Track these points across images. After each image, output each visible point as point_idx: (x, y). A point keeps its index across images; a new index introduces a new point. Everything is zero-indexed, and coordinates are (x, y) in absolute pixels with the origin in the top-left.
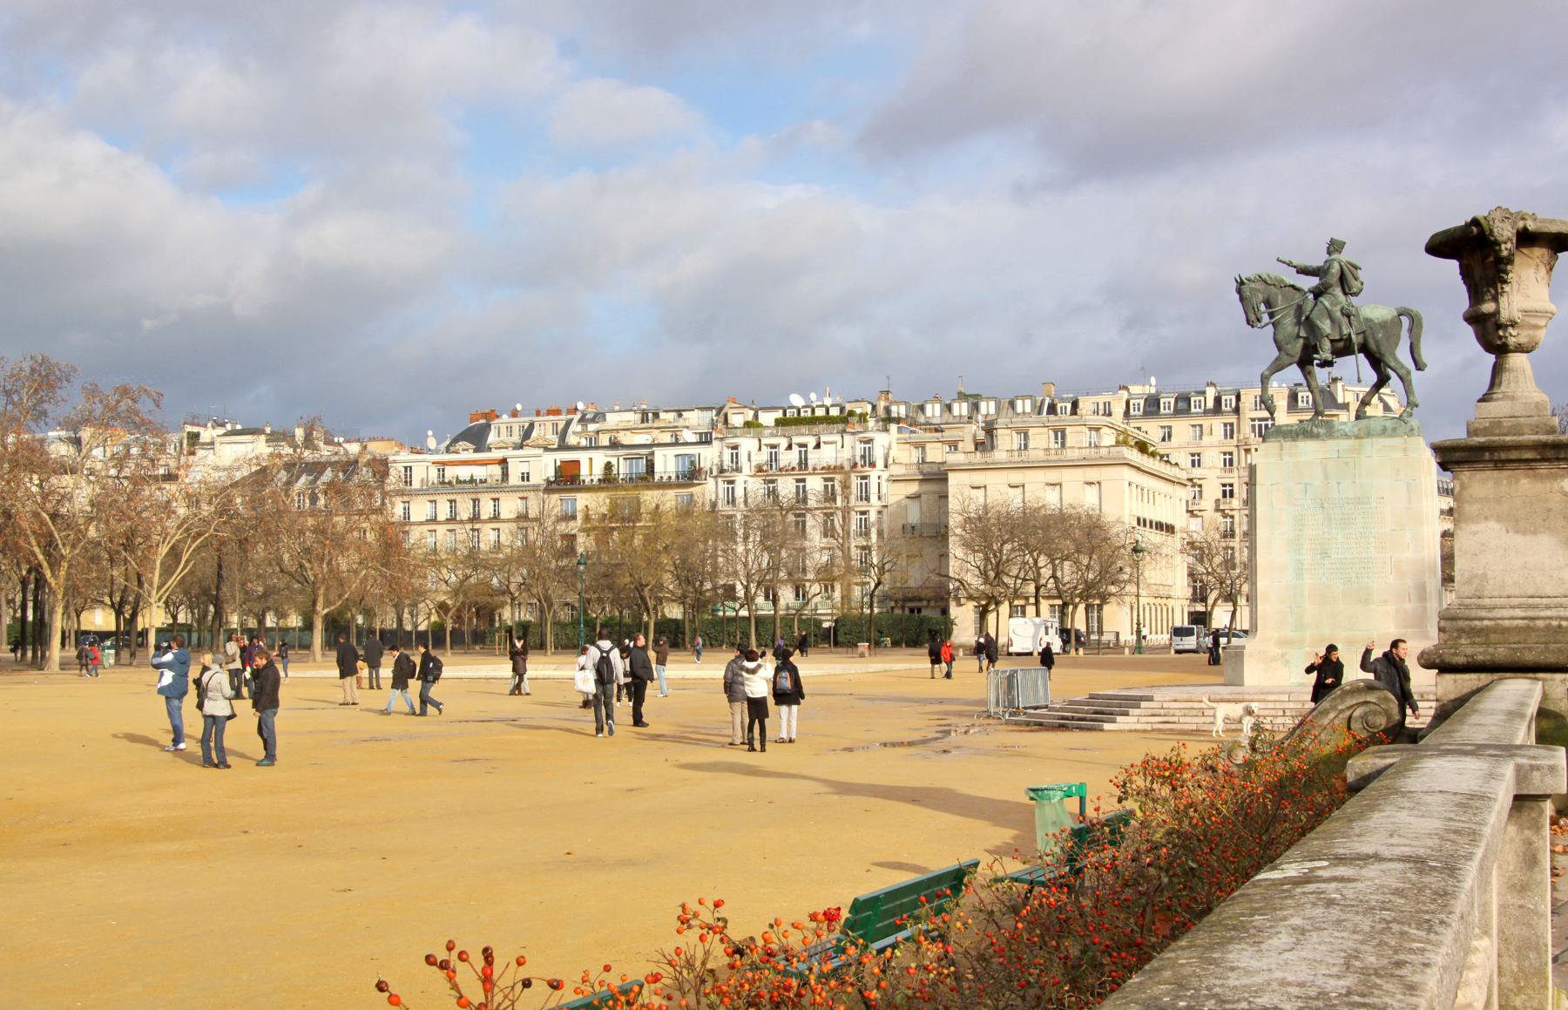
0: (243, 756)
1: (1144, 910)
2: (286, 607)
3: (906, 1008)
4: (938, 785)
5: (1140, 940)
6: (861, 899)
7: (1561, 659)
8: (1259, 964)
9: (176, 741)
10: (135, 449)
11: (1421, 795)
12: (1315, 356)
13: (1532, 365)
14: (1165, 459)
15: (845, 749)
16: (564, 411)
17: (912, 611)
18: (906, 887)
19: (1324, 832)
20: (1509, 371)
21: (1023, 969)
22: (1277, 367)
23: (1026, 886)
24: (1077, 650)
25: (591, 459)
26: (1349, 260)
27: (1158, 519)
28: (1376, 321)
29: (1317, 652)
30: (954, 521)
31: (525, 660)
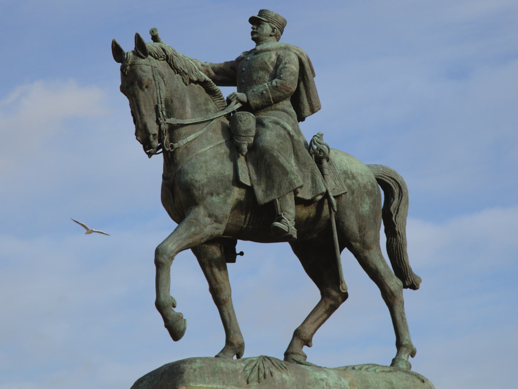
28: (303, 205)
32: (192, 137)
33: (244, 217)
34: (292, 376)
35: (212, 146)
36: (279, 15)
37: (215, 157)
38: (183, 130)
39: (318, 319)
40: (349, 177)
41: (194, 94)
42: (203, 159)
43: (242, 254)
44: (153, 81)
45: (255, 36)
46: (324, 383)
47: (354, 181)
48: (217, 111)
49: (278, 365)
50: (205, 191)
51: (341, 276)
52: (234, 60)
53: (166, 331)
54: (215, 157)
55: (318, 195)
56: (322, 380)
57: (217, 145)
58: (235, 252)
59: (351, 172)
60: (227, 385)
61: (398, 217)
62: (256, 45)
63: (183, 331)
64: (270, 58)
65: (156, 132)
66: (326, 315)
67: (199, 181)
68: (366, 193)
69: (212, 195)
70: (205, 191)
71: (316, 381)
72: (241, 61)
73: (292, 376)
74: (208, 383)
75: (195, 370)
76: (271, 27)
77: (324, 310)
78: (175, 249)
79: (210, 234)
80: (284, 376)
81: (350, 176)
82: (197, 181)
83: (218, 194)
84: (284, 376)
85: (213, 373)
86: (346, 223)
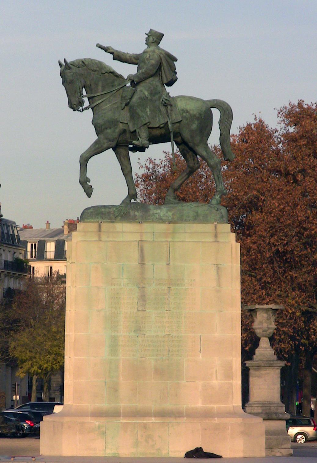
20: (300, 105)
34: (140, 213)
35: (110, 104)
37: (111, 110)
38: (96, 98)
39: (183, 178)
40: (184, 112)
42: (104, 112)
46: (158, 215)
47: (187, 114)
50: (103, 128)
53: (85, 193)
54: (111, 110)
55: (161, 125)
56: (157, 214)
57: (113, 104)
59: (186, 110)
60: (104, 219)
64: (147, 56)
66: (187, 176)
67: (100, 124)
68: (196, 119)
69: (107, 129)
70: (103, 128)
71: (153, 214)
73: (140, 213)
74: (94, 219)
75: (88, 213)
76: (153, 38)
77: (186, 173)
80: (136, 213)
81: (186, 111)
82: (98, 124)
83: (110, 128)
84: (136, 213)
85: (98, 214)
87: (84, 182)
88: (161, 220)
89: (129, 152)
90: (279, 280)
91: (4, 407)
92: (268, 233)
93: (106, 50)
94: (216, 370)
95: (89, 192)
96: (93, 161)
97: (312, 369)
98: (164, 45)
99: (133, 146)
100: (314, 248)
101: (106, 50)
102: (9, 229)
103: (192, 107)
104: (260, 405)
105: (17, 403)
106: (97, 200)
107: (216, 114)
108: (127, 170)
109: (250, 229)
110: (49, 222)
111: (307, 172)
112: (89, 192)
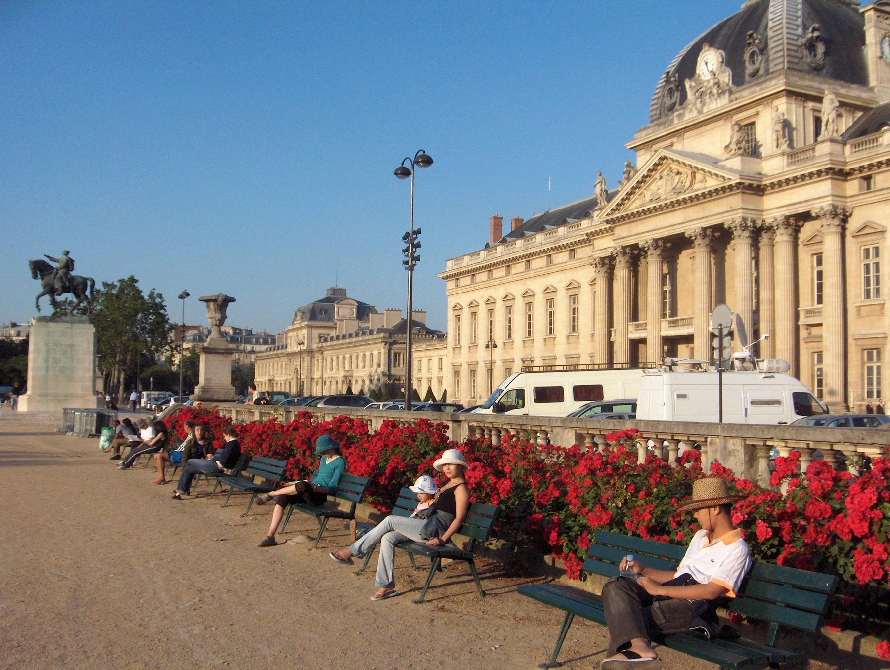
0: (727, 159)
1: (817, 133)
2: (474, 555)
3: (683, 669)
4: (91, 348)
5: (691, 526)
6: (839, 630)
7: (2, 437)
8: (393, 415)
9: (839, 511)
10: (330, 460)
11: (670, 161)
12: (234, 422)
13: (744, 577)
14: (61, 578)
15: (412, 262)
16: (820, 268)
17: (871, 552)
18: (28, 346)
19: (277, 368)
20: (761, 145)
21: (620, 476)
22: (43, 294)
23: (294, 391)
24: (212, 318)
25: (778, 402)
26: (206, 310)
27: (884, 270)
28: (863, 47)
29: (128, 471)
30: (338, 500)
31: (637, 637)
32: (574, 234)
33: (290, 334)
36: (581, 580)
41: (476, 449)
43: (67, 253)
44: (830, 120)
45: (344, 312)
48: (755, 245)
49: (282, 370)
51: (748, 10)
52: (683, 252)
58: (847, 652)
61: (434, 592)
62: (230, 304)
63: (825, 56)
65: (736, 201)
72: (702, 466)
78: (732, 138)
79: (712, 49)
86: (865, 52)
87: (38, 306)
88: (67, 322)
89: (492, 407)
90: (554, 451)
91: (826, 471)
92: (628, 472)
93: (48, 257)
94: (828, 121)
95: (39, 310)
96: (41, 299)
97: (879, 606)
98: (70, 256)
99: (717, 360)
100: (151, 407)
101: (48, 257)
102: (385, 358)
103: (80, 280)
104: (515, 588)
105: (792, 87)
106: (42, 314)
107: (89, 283)
108: (772, 156)
109: (162, 311)
110: (109, 282)
111: (295, 421)
112: (39, 310)
